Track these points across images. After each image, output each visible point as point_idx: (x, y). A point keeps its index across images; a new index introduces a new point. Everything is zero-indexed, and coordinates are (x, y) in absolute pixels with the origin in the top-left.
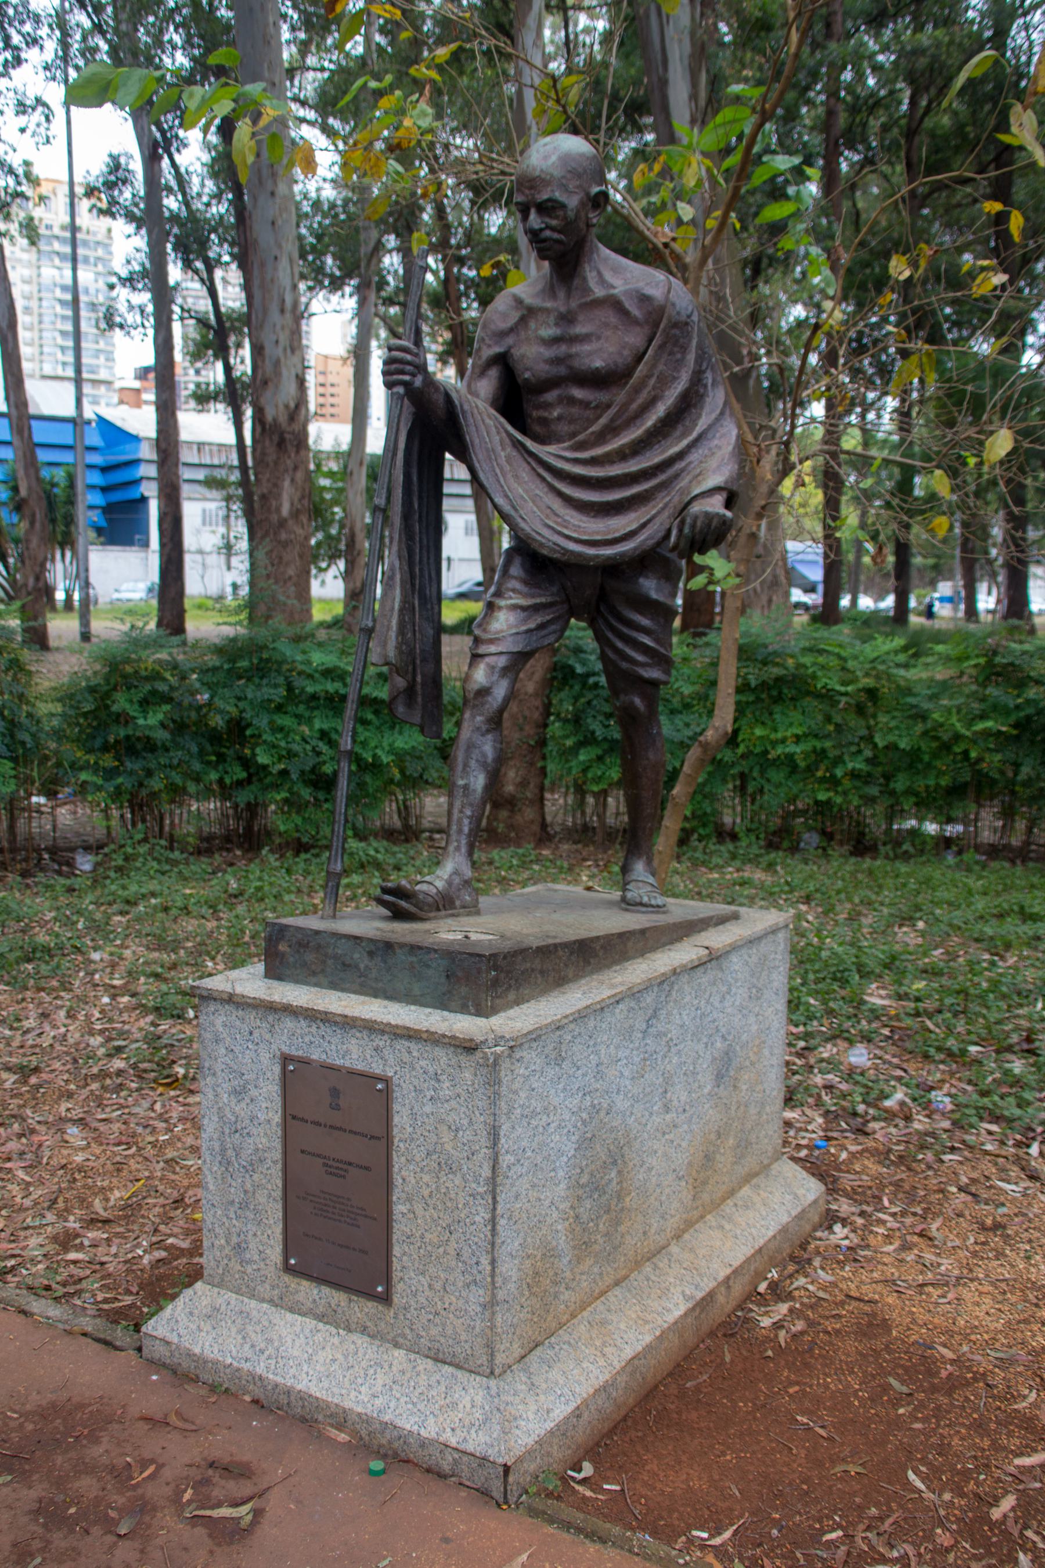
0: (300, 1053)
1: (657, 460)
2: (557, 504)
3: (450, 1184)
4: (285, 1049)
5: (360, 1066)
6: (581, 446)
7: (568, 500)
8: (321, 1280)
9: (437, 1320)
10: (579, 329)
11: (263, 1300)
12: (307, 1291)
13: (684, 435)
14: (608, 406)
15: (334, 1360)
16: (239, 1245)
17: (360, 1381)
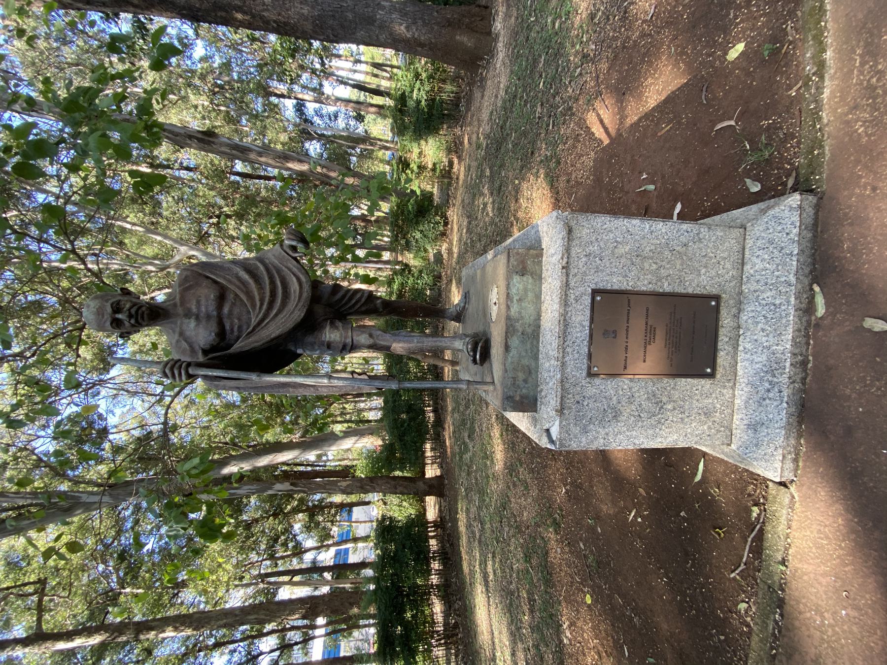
0: (585, 361)
1: (265, 273)
3: (648, 249)
4: (584, 373)
5: (588, 313)
6: (254, 306)
8: (715, 350)
9: (722, 263)
10: (194, 310)
11: (734, 396)
12: (722, 359)
13: (258, 268)
14: (236, 295)
15: (763, 330)
16: (705, 414)
17: (772, 307)
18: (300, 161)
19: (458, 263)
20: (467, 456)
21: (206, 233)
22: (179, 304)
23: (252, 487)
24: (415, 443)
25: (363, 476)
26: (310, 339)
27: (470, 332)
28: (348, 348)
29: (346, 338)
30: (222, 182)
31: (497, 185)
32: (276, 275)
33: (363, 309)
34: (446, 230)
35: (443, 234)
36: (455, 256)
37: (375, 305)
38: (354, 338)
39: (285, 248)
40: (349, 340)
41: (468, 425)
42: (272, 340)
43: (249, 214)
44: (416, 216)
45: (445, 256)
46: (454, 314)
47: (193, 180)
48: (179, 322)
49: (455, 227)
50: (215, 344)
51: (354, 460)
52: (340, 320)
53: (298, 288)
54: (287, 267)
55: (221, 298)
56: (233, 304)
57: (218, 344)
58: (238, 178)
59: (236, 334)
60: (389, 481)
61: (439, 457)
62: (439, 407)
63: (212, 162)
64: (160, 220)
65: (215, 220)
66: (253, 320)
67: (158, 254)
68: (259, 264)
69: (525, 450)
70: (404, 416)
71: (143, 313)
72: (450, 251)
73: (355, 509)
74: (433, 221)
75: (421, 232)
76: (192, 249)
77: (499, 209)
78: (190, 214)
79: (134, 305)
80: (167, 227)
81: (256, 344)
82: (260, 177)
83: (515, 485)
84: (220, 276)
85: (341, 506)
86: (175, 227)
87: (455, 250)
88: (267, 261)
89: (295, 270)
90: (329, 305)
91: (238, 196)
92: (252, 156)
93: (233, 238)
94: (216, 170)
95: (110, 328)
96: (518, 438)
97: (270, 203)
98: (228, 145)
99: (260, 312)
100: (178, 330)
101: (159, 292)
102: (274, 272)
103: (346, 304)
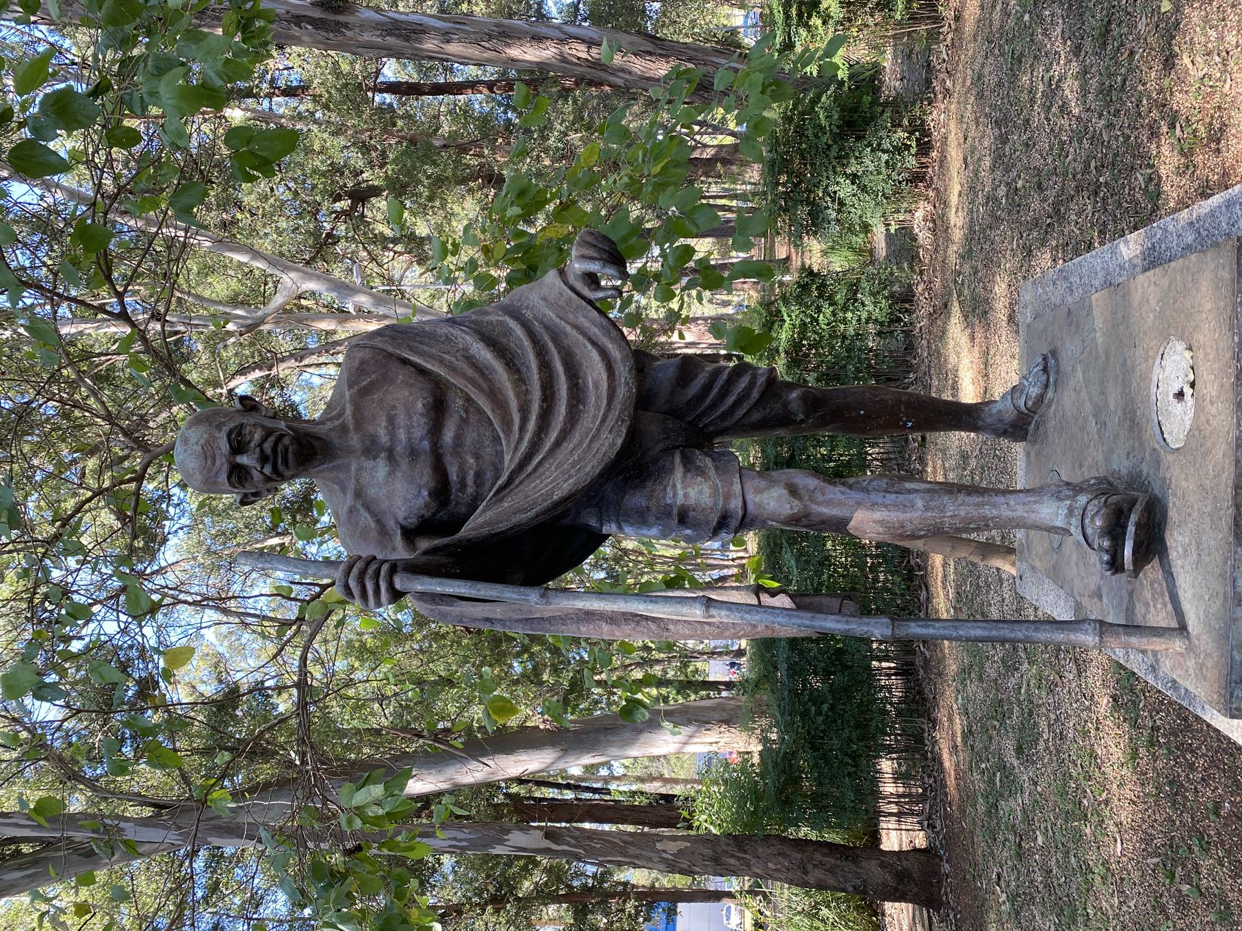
1: (527, 343)
2: (568, 446)
6: (507, 423)
7: (564, 435)
10: (384, 439)
13: (508, 332)
14: (468, 399)
18: (538, 38)
19: (967, 255)
20: (1013, 806)
21: (329, 235)
22: (351, 427)
23: (460, 835)
24: (855, 756)
25: (714, 831)
26: (636, 499)
27: (1090, 471)
28: (734, 523)
29: (727, 497)
30: (359, 114)
31: (1093, 23)
33: (756, 416)
34: (924, 166)
35: (917, 178)
36: (957, 235)
37: (786, 405)
38: (749, 497)
39: (572, 279)
40: (736, 504)
41: (1016, 718)
42: (557, 504)
43: (419, 182)
44: (839, 137)
45: (924, 237)
46: (1010, 415)
47: (300, 117)
48: (353, 467)
49: (955, 155)
50: (428, 514)
51: (676, 781)
52: (700, 446)
53: (604, 376)
54: (576, 327)
55: (438, 408)
56: (464, 421)
57: (434, 514)
58: (389, 98)
59: (470, 490)
60: (787, 850)
61: (922, 798)
62: (918, 661)
63: (337, 72)
64: (239, 216)
65: (344, 204)
66: (507, 458)
67: (237, 295)
68: (512, 324)
69: (1217, 808)
70: (816, 683)
71: (286, 450)
72: (938, 224)
73: (681, 907)
74: (886, 145)
75: (854, 178)
76: (309, 277)
77: (1105, 92)
78: (296, 193)
80: (253, 231)
81: (523, 517)
82: (438, 90)
83: (1182, 904)
84: (432, 357)
85: (651, 897)
87: (957, 219)
88: (529, 315)
89: (594, 331)
90: (674, 413)
91: (393, 142)
92: (430, 45)
93: (383, 241)
94: (346, 85)
95: (227, 486)
96: (1192, 767)
97: (463, 149)
98: (379, 27)
99: (521, 438)
100: (351, 485)
101: (242, 379)
102: (547, 338)
103: (714, 405)
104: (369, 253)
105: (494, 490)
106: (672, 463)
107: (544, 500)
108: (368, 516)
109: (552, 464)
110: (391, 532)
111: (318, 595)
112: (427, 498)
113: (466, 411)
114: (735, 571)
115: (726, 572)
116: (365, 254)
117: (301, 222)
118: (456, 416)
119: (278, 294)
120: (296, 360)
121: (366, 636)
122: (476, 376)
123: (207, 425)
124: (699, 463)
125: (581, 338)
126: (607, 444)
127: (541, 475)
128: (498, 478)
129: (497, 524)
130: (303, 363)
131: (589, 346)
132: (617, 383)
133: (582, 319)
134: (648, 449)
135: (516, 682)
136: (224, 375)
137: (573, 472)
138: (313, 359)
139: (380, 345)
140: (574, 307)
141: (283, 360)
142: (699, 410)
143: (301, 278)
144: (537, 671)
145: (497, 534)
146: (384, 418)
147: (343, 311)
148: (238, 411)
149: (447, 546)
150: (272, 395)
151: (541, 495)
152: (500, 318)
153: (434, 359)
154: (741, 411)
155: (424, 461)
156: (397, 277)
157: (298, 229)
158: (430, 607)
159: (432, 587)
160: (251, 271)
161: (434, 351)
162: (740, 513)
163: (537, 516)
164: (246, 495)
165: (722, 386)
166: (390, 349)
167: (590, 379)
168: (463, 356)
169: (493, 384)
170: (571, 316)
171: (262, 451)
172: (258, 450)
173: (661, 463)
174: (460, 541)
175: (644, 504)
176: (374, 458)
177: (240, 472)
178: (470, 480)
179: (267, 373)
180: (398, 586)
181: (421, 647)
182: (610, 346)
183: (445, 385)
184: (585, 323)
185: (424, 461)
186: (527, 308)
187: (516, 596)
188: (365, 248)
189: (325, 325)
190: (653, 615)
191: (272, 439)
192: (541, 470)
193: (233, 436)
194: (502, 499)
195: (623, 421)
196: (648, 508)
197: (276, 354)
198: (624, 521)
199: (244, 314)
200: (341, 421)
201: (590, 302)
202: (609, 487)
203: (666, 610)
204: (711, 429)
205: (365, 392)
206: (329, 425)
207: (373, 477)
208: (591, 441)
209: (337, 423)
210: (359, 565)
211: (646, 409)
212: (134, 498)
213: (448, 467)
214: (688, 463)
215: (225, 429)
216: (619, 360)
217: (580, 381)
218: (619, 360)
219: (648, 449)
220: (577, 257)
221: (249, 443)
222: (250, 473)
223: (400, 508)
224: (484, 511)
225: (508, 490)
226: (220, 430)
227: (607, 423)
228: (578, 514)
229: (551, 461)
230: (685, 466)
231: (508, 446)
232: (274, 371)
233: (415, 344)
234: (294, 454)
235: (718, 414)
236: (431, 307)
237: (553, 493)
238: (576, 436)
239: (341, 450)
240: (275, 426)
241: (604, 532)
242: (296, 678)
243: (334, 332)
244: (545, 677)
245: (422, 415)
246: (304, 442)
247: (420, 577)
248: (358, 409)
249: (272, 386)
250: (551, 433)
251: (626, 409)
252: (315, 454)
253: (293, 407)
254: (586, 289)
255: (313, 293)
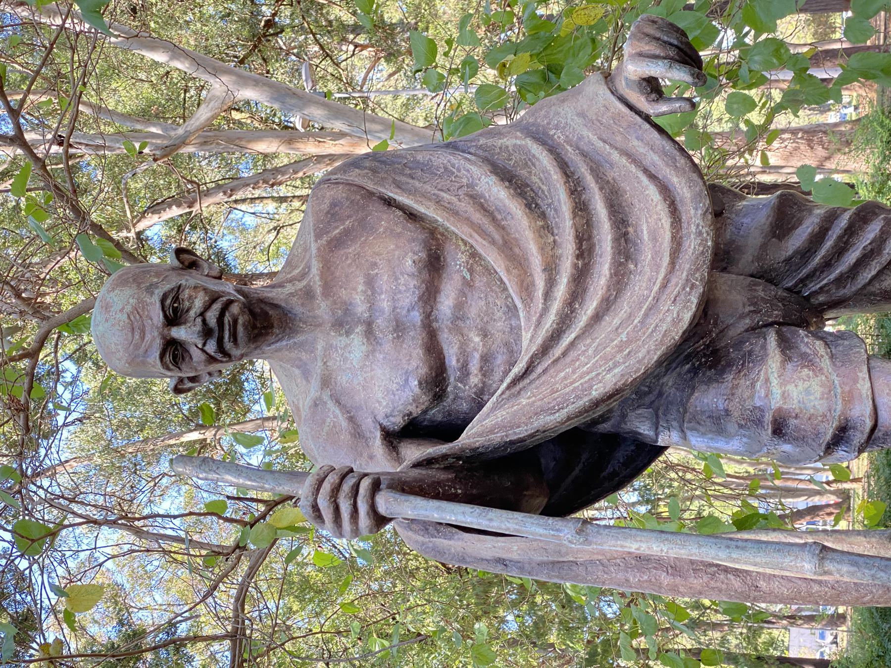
1: (556, 176)
2: (612, 321)
6: (527, 289)
7: (607, 305)
10: (361, 308)
13: (529, 161)
14: (474, 254)
21: (269, 24)
22: (319, 291)
32: (590, 181)
40: (861, 412)
42: (597, 403)
48: (320, 346)
50: (416, 411)
52: (803, 323)
56: (468, 284)
57: (425, 412)
59: (475, 380)
66: (526, 336)
68: (536, 149)
76: (244, 81)
79: (213, 301)
86: (189, 17)
88: (559, 137)
89: (653, 159)
93: (342, 30)
99: (545, 310)
100: (317, 369)
101: (155, 217)
103: (827, 265)
104: (322, 47)
105: (508, 380)
106: (764, 347)
107: (578, 397)
108: (338, 411)
109: (590, 345)
110: (368, 435)
111: (263, 516)
112: (417, 390)
113: (471, 271)
114: (832, 499)
115: (817, 500)
116: (317, 48)
117: (233, 7)
118: (457, 277)
119: (203, 106)
120: (225, 193)
121: (309, 569)
122: (485, 222)
123: (134, 286)
124: (803, 348)
125: (633, 168)
126: (669, 319)
127: (574, 361)
128: (513, 364)
129: (512, 427)
130: (233, 198)
131: (645, 180)
132: (684, 232)
133: (636, 143)
134: (728, 327)
135: (513, 643)
136: (132, 212)
137: (619, 358)
138: (249, 193)
139: (359, 181)
140: (625, 125)
141: (208, 193)
142: (805, 272)
143: (235, 83)
144: (540, 627)
145: (512, 443)
146: (361, 280)
147: (286, 127)
148: (174, 269)
149: (445, 457)
150: (193, 240)
151: (575, 388)
152: (518, 142)
153: (430, 200)
154: (867, 275)
155: (413, 338)
156: (359, 78)
157: (229, 15)
158: (420, 538)
159: (427, 513)
160: (168, 73)
161: (428, 187)
162: (869, 424)
163: (569, 418)
164: (181, 380)
165: (840, 238)
166: (371, 186)
167: (645, 227)
168: (467, 195)
169: (508, 234)
170: (619, 138)
171: (204, 321)
172: (199, 320)
173: (747, 347)
174: (462, 450)
175: (721, 407)
176: (348, 333)
177: (176, 349)
178: (474, 366)
179: (188, 210)
180: (382, 509)
181: (381, 586)
182: (675, 180)
183: (443, 235)
184: (638, 147)
185: (413, 338)
186: (557, 127)
187: (541, 531)
188: (317, 41)
189: (262, 147)
190: (737, 566)
191: (217, 306)
192: (573, 354)
193: (168, 301)
194: (519, 393)
195: (693, 287)
196: (727, 412)
197: (199, 185)
198: (692, 429)
199: (160, 132)
200: (304, 283)
201: (647, 118)
202: (669, 381)
203: (758, 560)
204: (821, 298)
205: (336, 244)
206: (289, 288)
207: (346, 359)
208: (646, 315)
209: (300, 285)
210: (332, 479)
211: (724, 270)
212: (26, 380)
213: (445, 347)
214: (785, 345)
215: (159, 293)
216: (688, 201)
217: (630, 229)
218: (688, 201)
219: (728, 327)
220: (632, 56)
221: (188, 311)
222: (188, 351)
223: (379, 402)
224: (493, 409)
225: (527, 381)
226: (152, 294)
227: (668, 290)
228: (624, 416)
229: (588, 341)
230: (783, 352)
231: (528, 319)
232: (196, 209)
233: (404, 179)
234: (246, 327)
235: (832, 277)
236: (402, 121)
237: (591, 388)
238: (624, 307)
239: (305, 323)
240: (222, 288)
241: (660, 443)
242: (229, 628)
243: (275, 155)
244: (552, 638)
245: (412, 275)
246: (258, 310)
247: (412, 498)
248: (327, 268)
249: (194, 227)
250: (588, 303)
251: (697, 270)
252: (272, 326)
253: (220, 255)
254: (643, 99)
255: (248, 103)
